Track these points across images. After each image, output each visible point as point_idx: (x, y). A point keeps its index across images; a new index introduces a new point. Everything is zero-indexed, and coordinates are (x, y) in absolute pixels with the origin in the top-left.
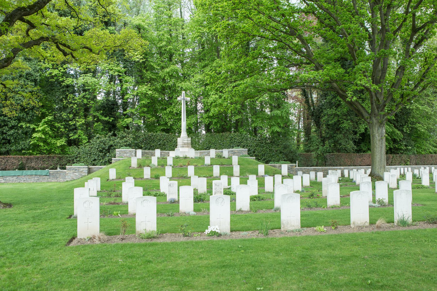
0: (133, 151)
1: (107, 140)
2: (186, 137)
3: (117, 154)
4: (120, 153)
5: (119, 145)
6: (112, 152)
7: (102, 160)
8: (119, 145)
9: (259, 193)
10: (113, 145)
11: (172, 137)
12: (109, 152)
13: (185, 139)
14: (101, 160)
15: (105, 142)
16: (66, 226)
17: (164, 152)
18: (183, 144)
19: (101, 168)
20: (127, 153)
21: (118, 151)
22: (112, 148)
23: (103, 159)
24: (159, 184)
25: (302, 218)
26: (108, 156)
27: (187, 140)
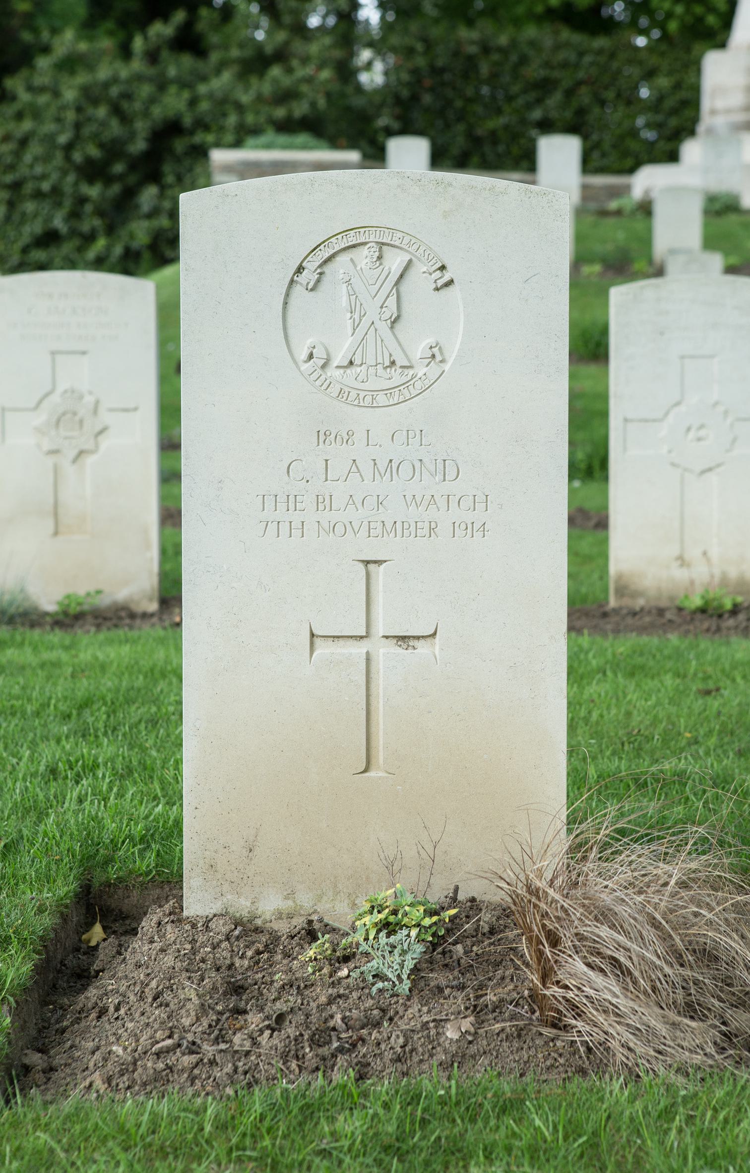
10: (187, 121)
12: (155, 177)
22: (180, 145)
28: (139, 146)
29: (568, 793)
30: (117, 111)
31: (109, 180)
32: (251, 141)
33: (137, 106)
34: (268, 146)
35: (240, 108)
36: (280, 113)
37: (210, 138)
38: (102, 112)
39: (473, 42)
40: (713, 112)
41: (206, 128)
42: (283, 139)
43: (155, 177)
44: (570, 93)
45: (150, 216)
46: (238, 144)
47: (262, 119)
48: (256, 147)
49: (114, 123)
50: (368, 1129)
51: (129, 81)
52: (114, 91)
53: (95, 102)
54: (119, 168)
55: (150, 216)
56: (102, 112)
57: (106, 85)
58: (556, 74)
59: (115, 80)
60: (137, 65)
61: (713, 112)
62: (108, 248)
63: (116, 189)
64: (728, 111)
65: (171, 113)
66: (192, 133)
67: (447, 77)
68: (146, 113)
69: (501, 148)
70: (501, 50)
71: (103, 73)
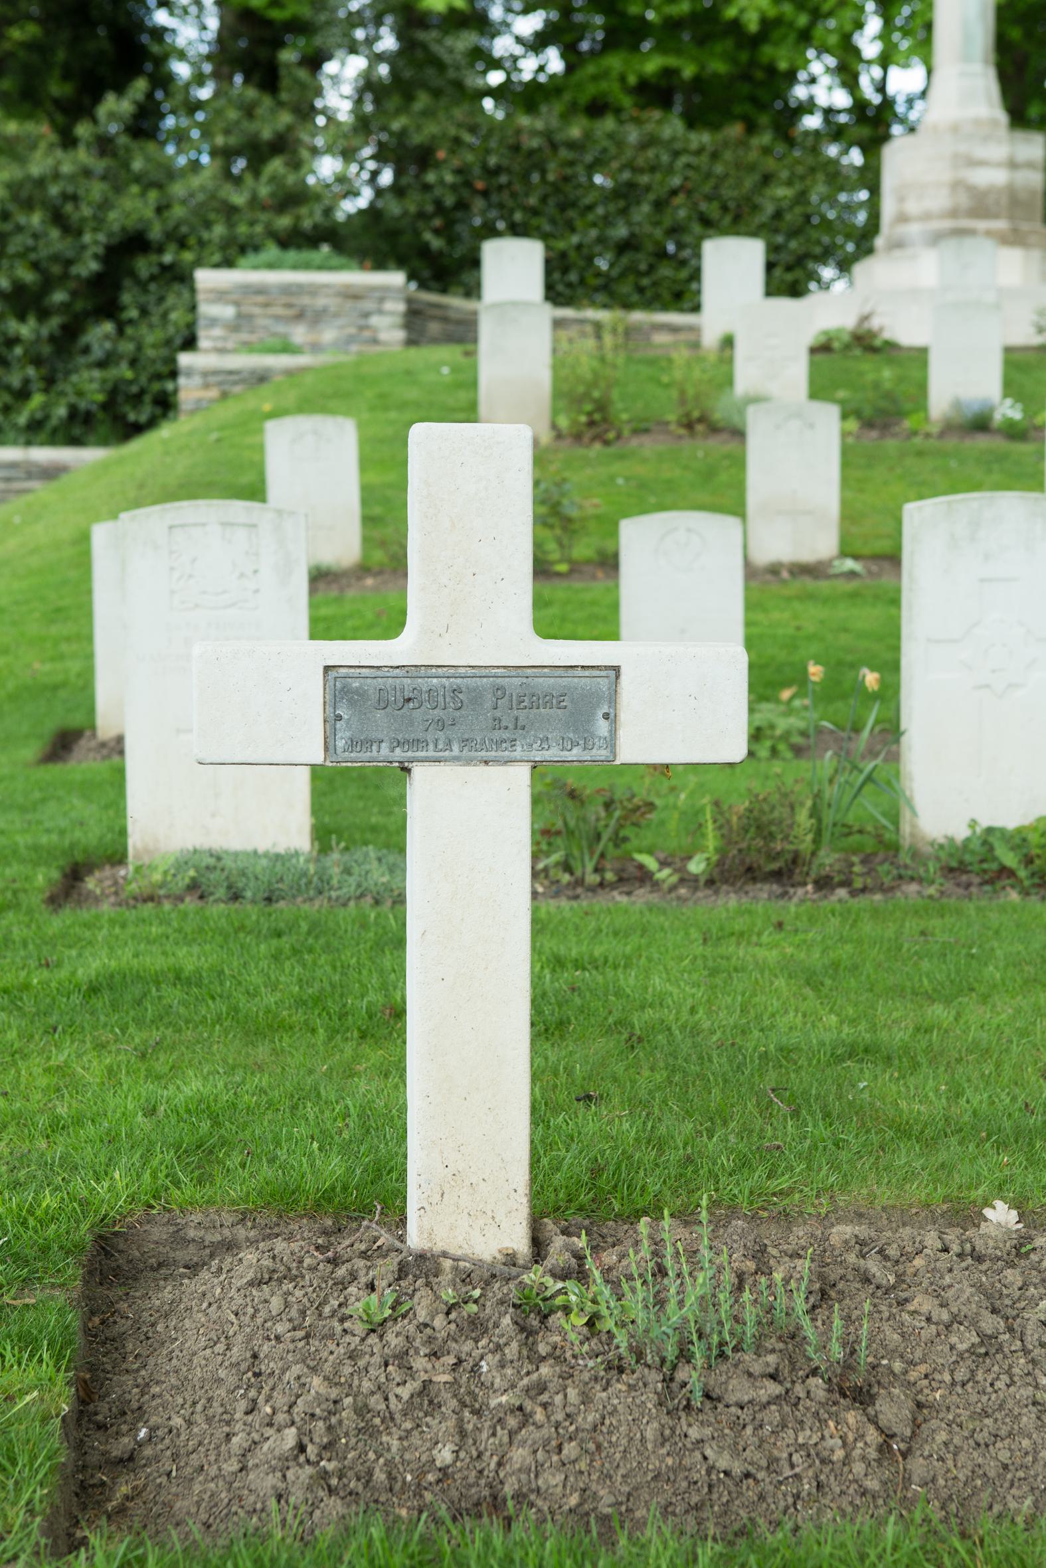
0: (383, 293)
1: (87, 173)
2: (994, 122)
3: (213, 322)
4: (241, 322)
5: (219, 230)
6: (144, 312)
7: (37, 400)
8: (219, 230)
9: (323, 835)
10: (156, 233)
11: (752, 168)
12: (109, 309)
13: (980, 152)
14: (23, 394)
15: (66, 197)
16: (532, 1475)
17: (674, 329)
18: (964, 200)
19: (50, 473)
20: (316, 318)
21: (221, 296)
22: (144, 266)
23: (49, 382)
24: (898, 591)
25: (550, 944)
26: (97, 353)
27: (1013, 165)
28: (90, 266)
29: (325, 742)
30: (58, 218)
31: (44, 314)
32: (252, 258)
33: (87, 211)
34: (271, 266)
35: (230, 211)
36: (284, 222)
37: (188, 256)
38: (36, 219)
39: (534, 133)
40: (903, 218)
41: (183, 244)
42: (292, 255)
43: (109, 309)
44: (659, 205)
45: (102, 364)
46: (228, 263)
47: (259, 229)
48: (256, 267)
49: (55, 233)
50: (243, 1082)
51: (72, 178)
52: (54, 190)
53: (28, 205)
54: (59, 296)
55: (102, 364)
56: (36, 219)
57: (41, 183)
58: (644, 179)
59: (56, 176)
60: (83, 155)
61: (903, 218)
62: (45, 407)
63: (55, 322)
64: (927, 217)
65: (130, 223)
66: (160, 250)
67: (503, 179)
68: (99, 222)
69: (573, 277)
70: (572, 145)
71: (38, 166)
